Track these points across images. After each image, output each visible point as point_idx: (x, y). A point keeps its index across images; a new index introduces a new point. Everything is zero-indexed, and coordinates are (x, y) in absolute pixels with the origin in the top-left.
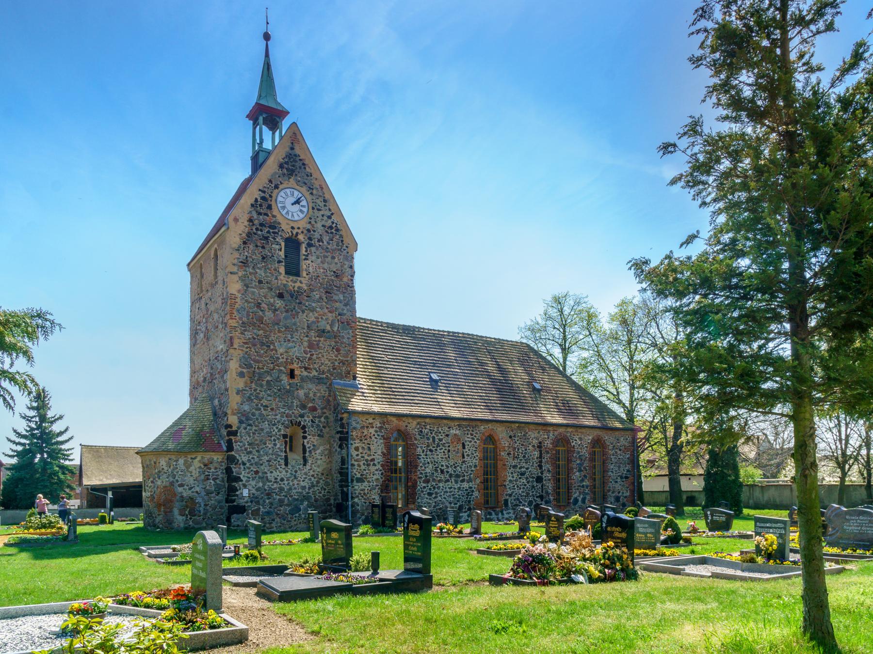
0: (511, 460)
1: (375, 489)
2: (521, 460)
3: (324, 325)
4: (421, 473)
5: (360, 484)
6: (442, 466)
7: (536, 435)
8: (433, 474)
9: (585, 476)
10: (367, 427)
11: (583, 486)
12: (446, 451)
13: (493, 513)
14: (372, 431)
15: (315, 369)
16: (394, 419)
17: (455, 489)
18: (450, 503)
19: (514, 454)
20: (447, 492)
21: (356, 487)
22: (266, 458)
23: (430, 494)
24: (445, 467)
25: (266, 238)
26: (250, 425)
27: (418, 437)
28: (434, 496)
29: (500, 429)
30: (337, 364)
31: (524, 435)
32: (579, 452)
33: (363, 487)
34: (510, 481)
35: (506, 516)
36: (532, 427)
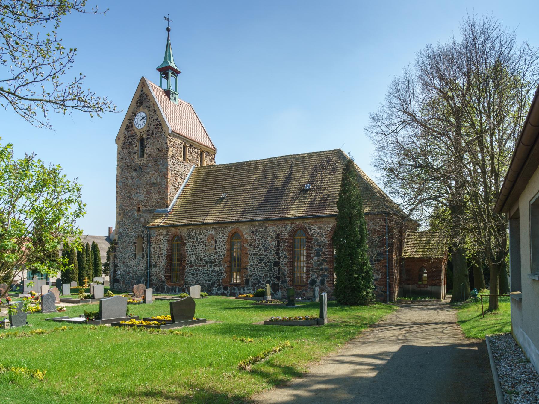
0: (252, 249)
1: (162, 271)
2: (260, 249)
3: (153, 180)
4: (188, 261)
5: (154, 268)
6: (201, 256)
7: (275, 228)
8: (195, 261)
9: (324, 260)
10: (159, 235)
11: (322, 269)
12: (204, 246)
13: (237, 289)
14: (161, 237)
15: (149, 205)
16: (173, 229)
17: (210, 271)
18: (206, 281)
19: (255, 245)
20: (204, 273)
21: (153, 270)
22: (128, 255)
23: (193, 274)
24: (203, 257)
25: (131, 143)
26: (122, 239)
27: (187, 238)
28: (195, 275)
29: (244, 227)
30: (159, 200)
31: (264, 230)
32: (317, 240)
33: (156, 270)
34: (251, 265)
35: (246, 291)
36: (269, 222)
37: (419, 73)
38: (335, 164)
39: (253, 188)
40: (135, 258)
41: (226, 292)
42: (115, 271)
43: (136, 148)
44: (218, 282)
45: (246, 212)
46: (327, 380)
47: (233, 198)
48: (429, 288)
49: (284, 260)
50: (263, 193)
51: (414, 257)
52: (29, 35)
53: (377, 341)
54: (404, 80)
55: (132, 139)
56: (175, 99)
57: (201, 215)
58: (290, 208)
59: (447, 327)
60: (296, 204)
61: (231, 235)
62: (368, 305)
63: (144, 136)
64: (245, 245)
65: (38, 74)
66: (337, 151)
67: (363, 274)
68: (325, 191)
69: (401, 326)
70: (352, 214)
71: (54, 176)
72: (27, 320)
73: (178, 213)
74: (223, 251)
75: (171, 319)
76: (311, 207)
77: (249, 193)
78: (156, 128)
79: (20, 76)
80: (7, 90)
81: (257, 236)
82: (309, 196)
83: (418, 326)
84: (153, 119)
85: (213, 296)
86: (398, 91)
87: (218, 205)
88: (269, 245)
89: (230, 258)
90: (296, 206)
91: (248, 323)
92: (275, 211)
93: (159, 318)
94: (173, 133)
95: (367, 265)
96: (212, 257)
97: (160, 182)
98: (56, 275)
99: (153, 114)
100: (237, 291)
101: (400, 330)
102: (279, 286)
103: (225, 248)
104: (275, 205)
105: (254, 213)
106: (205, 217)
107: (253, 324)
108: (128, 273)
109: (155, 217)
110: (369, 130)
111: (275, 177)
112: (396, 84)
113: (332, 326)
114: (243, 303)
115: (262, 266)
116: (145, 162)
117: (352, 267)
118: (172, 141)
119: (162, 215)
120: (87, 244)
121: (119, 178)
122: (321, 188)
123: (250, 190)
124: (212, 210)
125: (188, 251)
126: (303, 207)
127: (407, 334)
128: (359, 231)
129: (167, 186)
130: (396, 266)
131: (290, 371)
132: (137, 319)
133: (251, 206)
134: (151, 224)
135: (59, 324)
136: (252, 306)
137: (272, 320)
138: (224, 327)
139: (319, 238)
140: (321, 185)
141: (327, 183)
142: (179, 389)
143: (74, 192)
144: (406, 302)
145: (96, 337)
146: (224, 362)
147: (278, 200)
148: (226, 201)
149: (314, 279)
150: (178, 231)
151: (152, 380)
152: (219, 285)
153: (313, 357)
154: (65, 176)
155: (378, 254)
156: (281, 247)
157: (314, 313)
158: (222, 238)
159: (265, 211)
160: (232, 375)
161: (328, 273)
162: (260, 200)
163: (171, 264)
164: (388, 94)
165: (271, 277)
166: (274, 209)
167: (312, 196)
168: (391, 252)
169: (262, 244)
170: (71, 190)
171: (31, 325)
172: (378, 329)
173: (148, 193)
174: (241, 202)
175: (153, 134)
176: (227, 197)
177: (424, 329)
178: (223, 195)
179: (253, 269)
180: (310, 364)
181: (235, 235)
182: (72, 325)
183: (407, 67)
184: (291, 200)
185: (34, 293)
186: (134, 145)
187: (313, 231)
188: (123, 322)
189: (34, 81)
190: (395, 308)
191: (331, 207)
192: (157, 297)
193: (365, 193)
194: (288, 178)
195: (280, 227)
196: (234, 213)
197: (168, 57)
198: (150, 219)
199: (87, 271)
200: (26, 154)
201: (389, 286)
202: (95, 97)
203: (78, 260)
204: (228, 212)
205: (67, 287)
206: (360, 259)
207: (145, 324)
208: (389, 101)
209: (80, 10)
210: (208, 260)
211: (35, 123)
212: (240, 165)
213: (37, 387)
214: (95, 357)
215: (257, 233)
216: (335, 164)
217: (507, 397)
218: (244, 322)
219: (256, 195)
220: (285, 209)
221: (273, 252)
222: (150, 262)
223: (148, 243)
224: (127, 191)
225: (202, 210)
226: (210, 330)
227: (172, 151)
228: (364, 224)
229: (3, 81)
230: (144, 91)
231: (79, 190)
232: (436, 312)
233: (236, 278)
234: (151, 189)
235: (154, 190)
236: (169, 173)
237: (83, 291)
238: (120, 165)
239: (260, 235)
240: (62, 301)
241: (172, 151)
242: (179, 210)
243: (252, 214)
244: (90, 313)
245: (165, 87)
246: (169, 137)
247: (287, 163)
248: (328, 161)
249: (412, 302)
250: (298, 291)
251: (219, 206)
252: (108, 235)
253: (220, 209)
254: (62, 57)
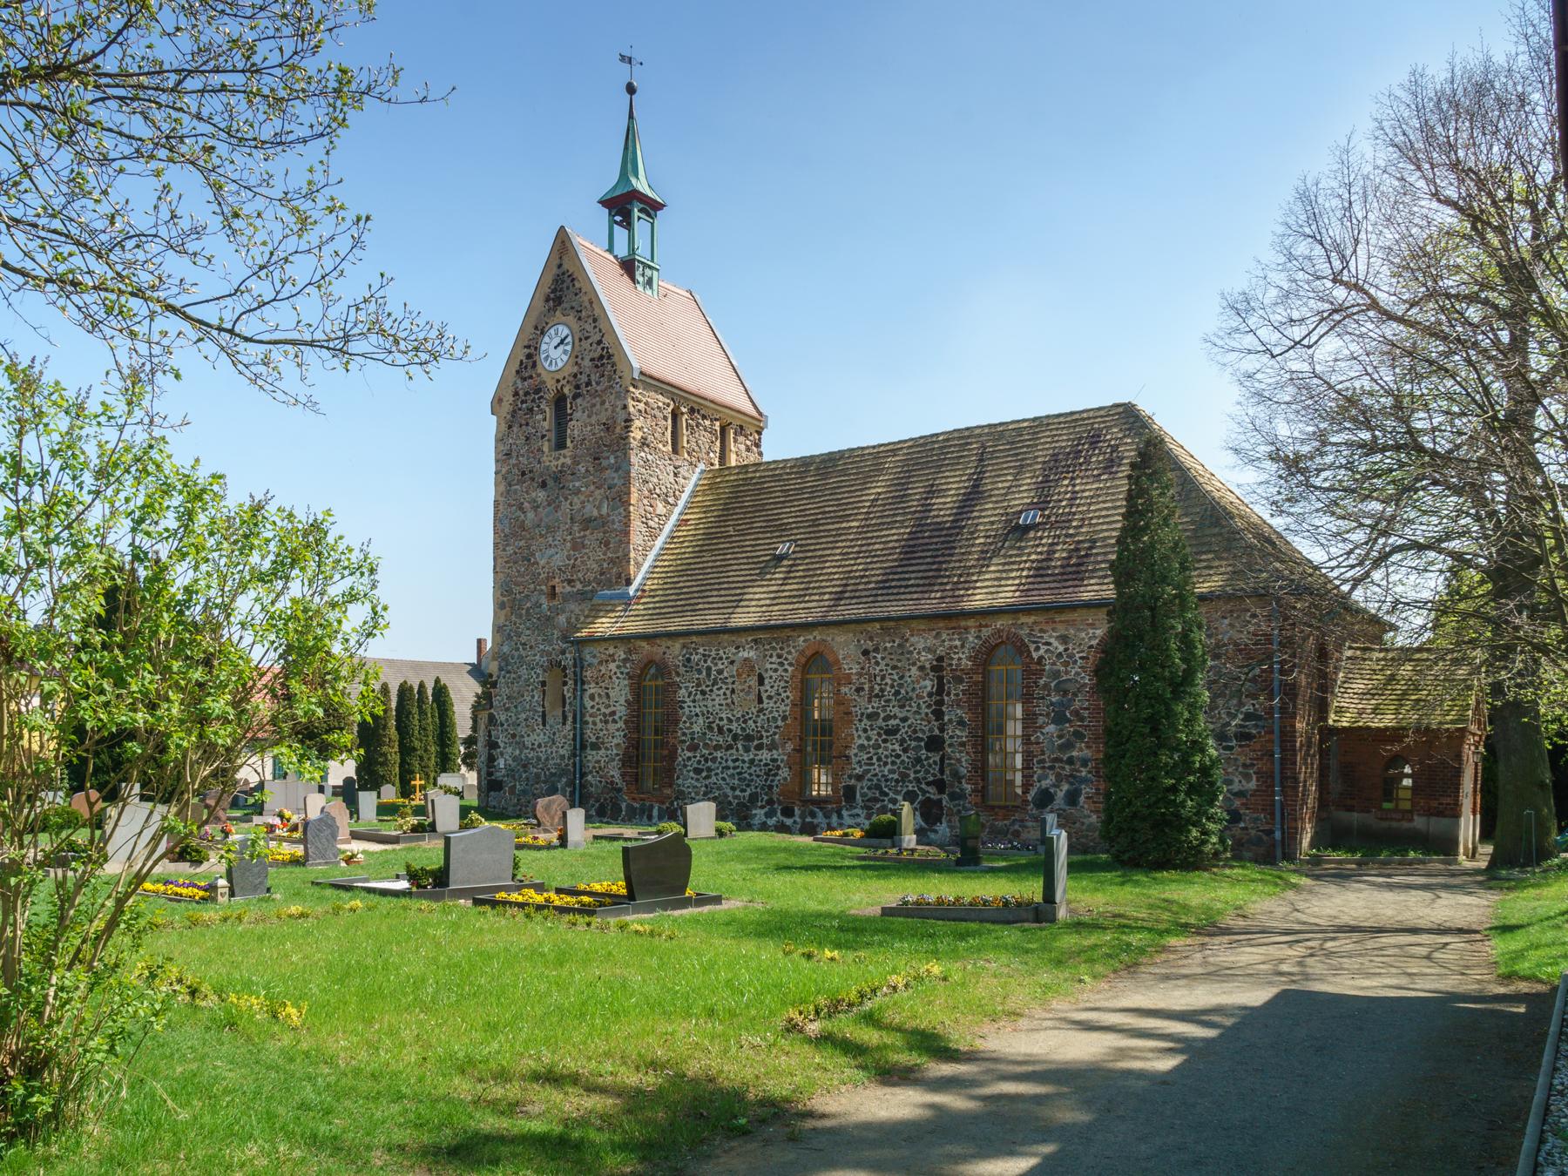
0: (863, 702)
1: (614, 760)
2: (888, 701)
4: (684, 734)
6: (721, 719)
7: (931, 642)
9: (1078, 735)
10: (607, 661)
11: (1070, 761)
12: (728, 692)
13: (820, 814)
14: (612, 666)
16: (644, 644)
17: (744, 762)
18: (733, 789)
19: (872, 689)
20: (728, 768)
21: (590, 758)
22: (523, 716)
23: (698, 771)
24: (725, 721)
25: (531, 410)
26: (509, 672)
27: (682, 670)
28: (704, 774)
29: (841, 639)
30: (605, 565)
31: (899, 645)
32: (1056, 674)
34: (862, 747)
35: (848, 820)
36: (914, 624)
37: (1386, 154)
38: (1115, 449)
39: (868, 526)
40: (544, 725)
41: (789, 822)
42: (491, 759)
43: (546, 425)
44: (766, 794)
45: (847, 595)
46: (1034, 1072)
47: (810, 554)
48: (1419, 822)
49: (958, 732)
50: (896, 541)
51: (1369, 728)
52: (266, 177)
53: (1209, 974)
54: (1335, 184)
55: (533, 401)
56: (650, 282)
57: (721, 605)
58: (976, 581)
59: (1447, 944)
60: (992, 568)
61: (803, 660)
62: (1205, 870)
63: (566, 390)
64: (844, 690)
65: (283, 282)
66: (1121, 409)
67: (1191, 778)
68: (1084, 530)
69: (1294, 934)
70: (1157, 599)
71: (316, 540)
72: (269, 883)
73: (657, 599)
74: (780, 706)
75: (624, 891)
76: (1039, 579)
77: (858, 539)
78: (597, 366)
79: (242, 288)
80: (215, 322)
81: (877, 663)
82: (1033, 546)
83: (1350, 938)
84: (590, 341)
85: (751, 834)
86: (1314, 217)
87: (768, 576)
88: (914, 689)
89: (801, 724)
90: (993, 576)
91: (835, 911)
92: (932, 592)
93: (597, 887)
94: (643, 378)
95: (1203, 751)
96: (750, 722)
97: (608, 515)
98: (342, 769)
99: (589, 327)
100: (820, 819)
101: (1290, 947)
102: (941, 808)
103: (788, 697)
104: (931, 574)
105: (871, 599)
106: (730, 610)
107: (852, 912)
108: (525, 766)
109: (596, 612)
110: (1220, 343)
111: (932, 492)
112: (1307, 199)
113: (1078, 926)
114: (833, 855)
115: (893, 750)
116: (568, 461)
117: (1156, 754)
118: (640, 402)
119: (615, 605)
120: (422, 685)
121: (501, 507)
122: (1070, 521)
123: (860, 533)
124: (750, 590)
125: (685, 705)
126: (1014, 578)
127: (1310, 961)
128: (1179, 649)
129: (627, 524)
130: (1307, 754)
131: (933, 1045)
132: (540, 888)
133: (862, 577)
134: (584, 633)
135: (344, 895)
136: (856, 863)
137: (906, 903)
138: (766, 917)
139: (1062, 668)
140: (1069, 514)
141: (1090, 504)
142: (623, 1069)
143: (362, 574)
144: (1340, 862)
145: (430, 931)
146: (747, 1006)
147: (940, 559)
148: (791, 566)
149: (1047, 789)
150: (657, 650)
151: (556, 1043)
152: (770, 802)
153: (1000, 1008)
154: (341, 538)
155: (1248, 717)
156: (948, 694)
157: (1031, 889)
158: (779, 670)
159: (902, 590)
160: (763, 1044)
161: (1090, 772)
162: (887, 561)
163: (638, 742)
164: (1281, 229)
165: (918, 780)
166: (928, 586)
167: (1043, 545)
168: (1288, 715)
169: (892, 686)
170: (356, 570)
171: (278, 896)
172: (1217, 940)
173: (577, 546)
174: (834, 567)
175: (588, 384)
176: (794, 552)
177: (1370, 944)
178: (782, 549)
179: (865, 757)
180: (988, 1027)
181: (816, 663)
182: (374, 899)
183: (1343, 143)
184: (978, 560)
185: (287, 814)
186: (540, 417)
187: (1043, 648)
188: (503, 895)
189: (274, 300)
190: (1294, 879)
191: (1100, 577)
192: (599, 832)
193: (1208, 532)
194: (970, 493)
195: (944, 636)
196: (813, 598)
197: (629, 165)
198: (582, 619)
199: (421, 758)
200: (251, 496)
201: (1283, 814)
202: (421, 321)
203: (398, 728)
204: (794, 597)
205: (367, 801)
206: (1182, 731)
207: (557, 903)
208: (1285, 252)
209: (386, 97)
210: (739, 731)
211: (279, 395)
212: (830, 460)
213: (286, 1043)
214: (423, 980)
215: (879, 656)
216: (1115, 449)
217: (1554, 1147)
218: (824, 908)
219: (877, 546)
220: (961, 586)
221: (924, 710)
222: (582, 734)
223: (576, 684)
224: (522, 543)
225: (723, 592)
226: (728, 924)
227: (641, 429)
228: (1195, 629)
229: (207, 301)
230: (565, 267)
231: (372, 571)
232: (1428, 895)
233: (821, 783)
234: (585, 536)
235: (592, 538)
236: (632, 489)
237: (410, 812)
238: (504, 470)
239: (887, 661)
240: (356, 836)
241: (641, 429)
242: (660, 592)
243: (864, 600)
244: (422, 869)
245: (622, 250)
246: (632, 389)
247: (969, 450)
248: (1095, 440)
249: (1359, 864)
250: (999, 824)
251: (771, 580)
252: (474, 660)
253: (775, 588)
254: (340, 229)
